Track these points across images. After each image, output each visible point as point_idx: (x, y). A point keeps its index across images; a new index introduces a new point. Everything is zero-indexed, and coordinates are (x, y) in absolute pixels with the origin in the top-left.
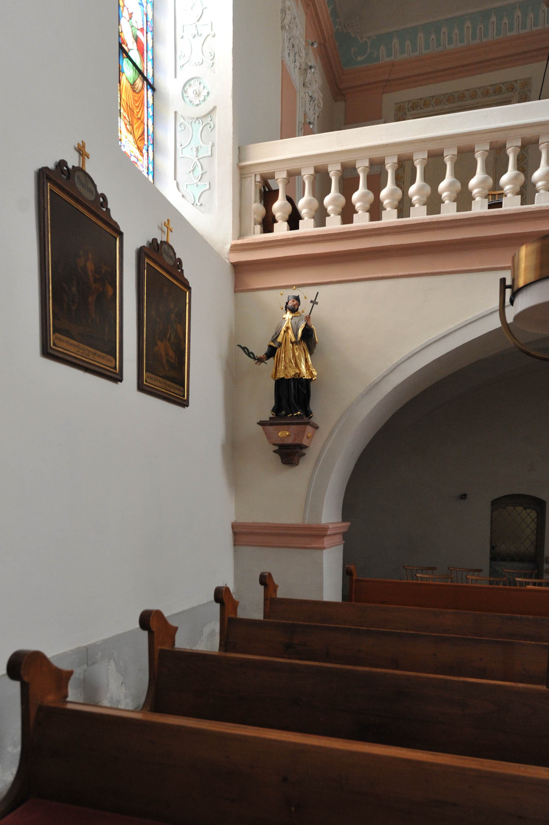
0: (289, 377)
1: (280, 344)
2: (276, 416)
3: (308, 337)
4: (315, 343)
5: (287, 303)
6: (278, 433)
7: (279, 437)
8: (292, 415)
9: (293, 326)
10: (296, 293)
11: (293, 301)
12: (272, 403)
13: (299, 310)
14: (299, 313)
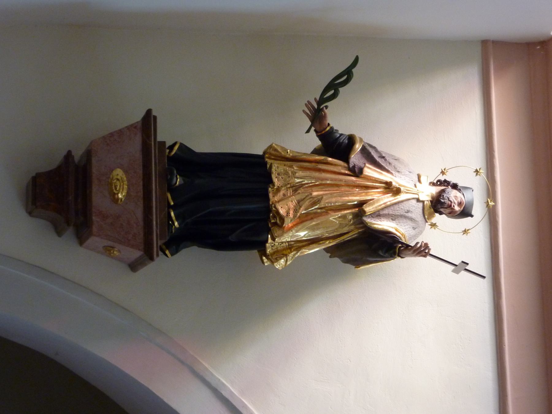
0: (273, 198)
1: (357, 172)
2: (169, 158)
3: (371, 246)
4: (358, 262)
5: (455, 186)
6: (121, 167)
7: (112, 171)
8: (170, 207)
9: (401, 206)
10: (478, 210)
11: (460, 204)
12: (202, 145)
13: (437, 215)
14: (431, 216)
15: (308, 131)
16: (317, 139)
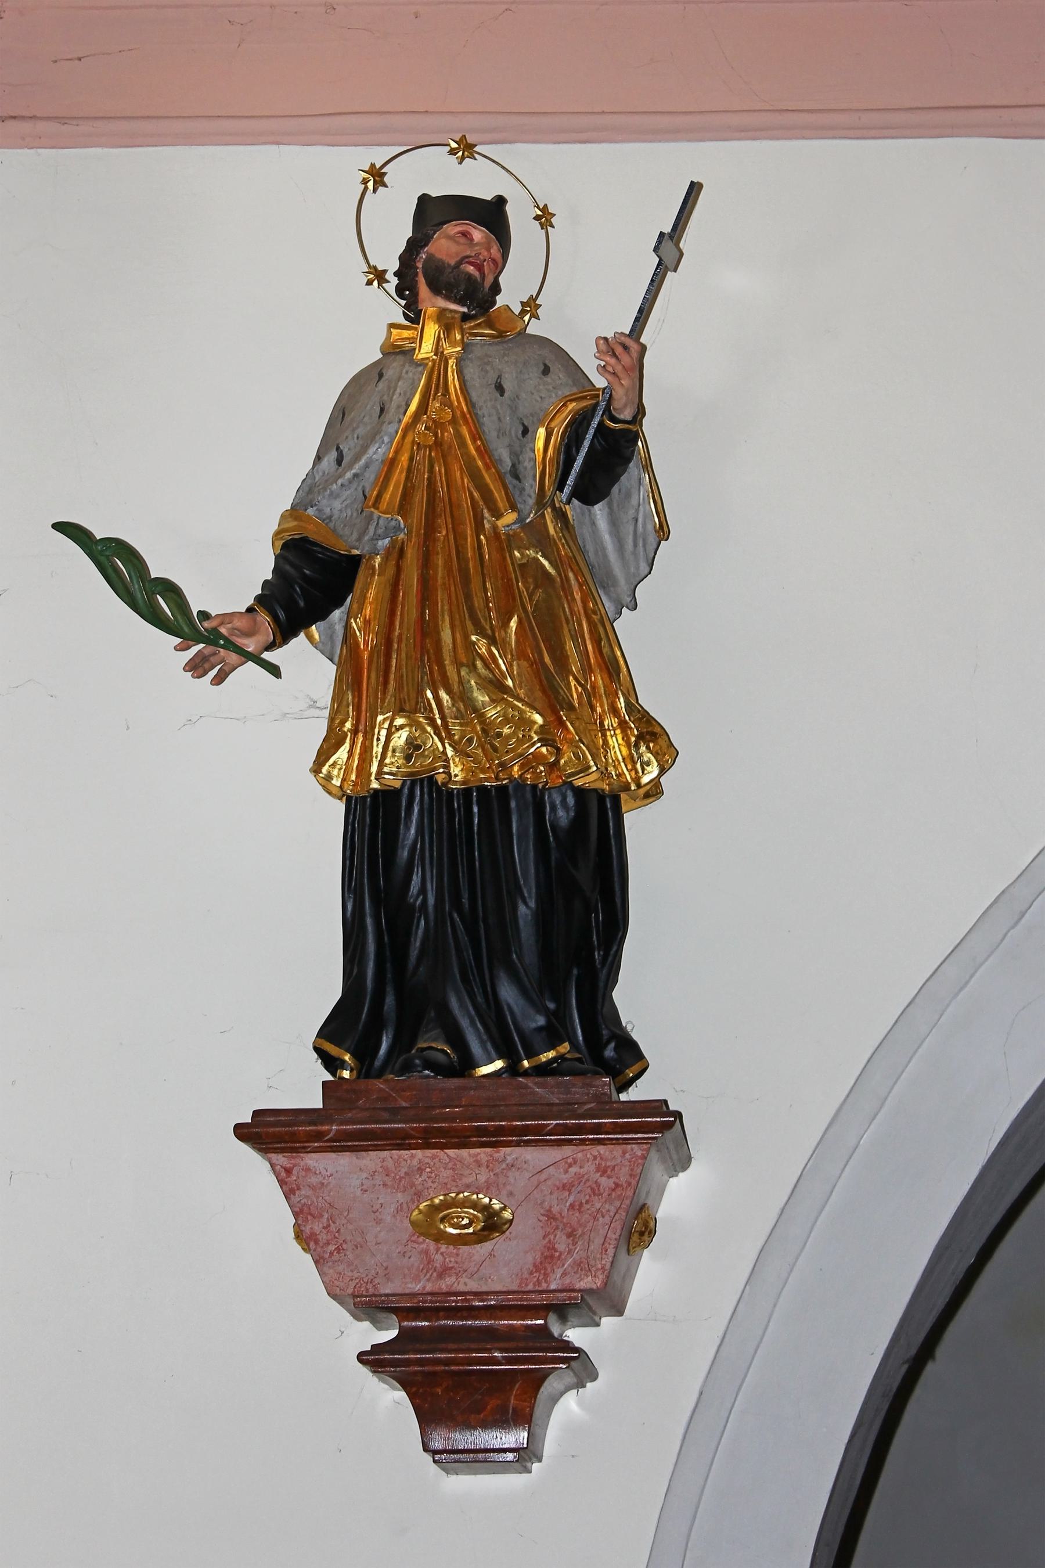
12: (317, 978)
13: (500, 301)
15: (274, 670)
16: (294, 642)
